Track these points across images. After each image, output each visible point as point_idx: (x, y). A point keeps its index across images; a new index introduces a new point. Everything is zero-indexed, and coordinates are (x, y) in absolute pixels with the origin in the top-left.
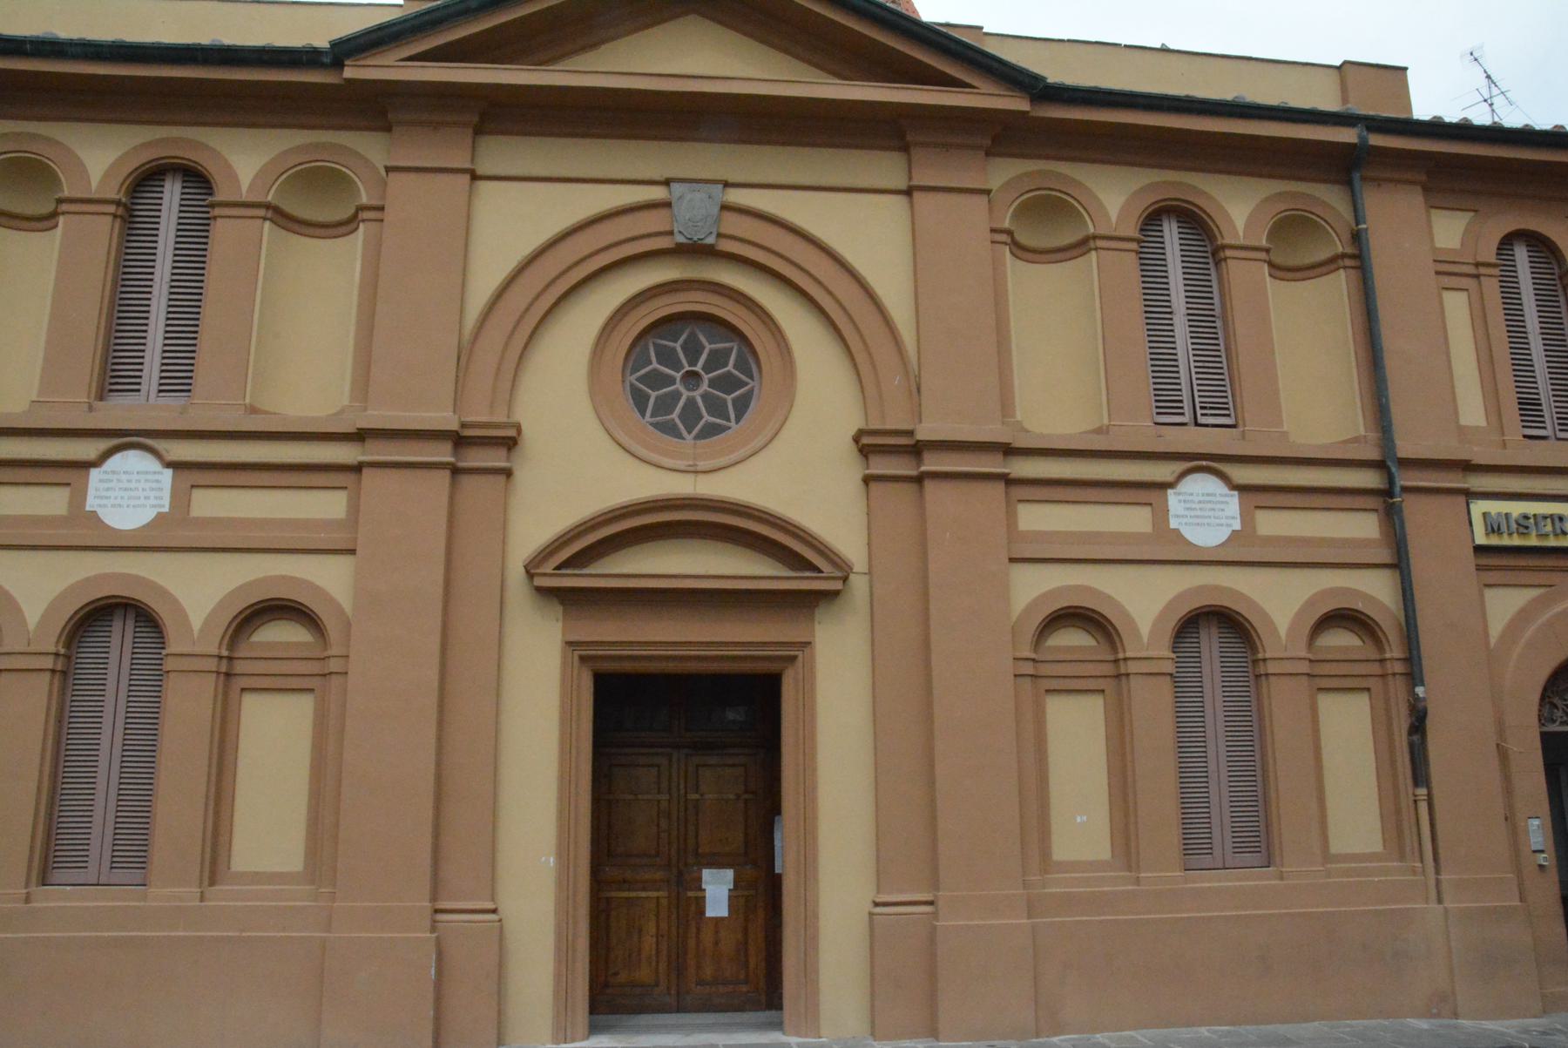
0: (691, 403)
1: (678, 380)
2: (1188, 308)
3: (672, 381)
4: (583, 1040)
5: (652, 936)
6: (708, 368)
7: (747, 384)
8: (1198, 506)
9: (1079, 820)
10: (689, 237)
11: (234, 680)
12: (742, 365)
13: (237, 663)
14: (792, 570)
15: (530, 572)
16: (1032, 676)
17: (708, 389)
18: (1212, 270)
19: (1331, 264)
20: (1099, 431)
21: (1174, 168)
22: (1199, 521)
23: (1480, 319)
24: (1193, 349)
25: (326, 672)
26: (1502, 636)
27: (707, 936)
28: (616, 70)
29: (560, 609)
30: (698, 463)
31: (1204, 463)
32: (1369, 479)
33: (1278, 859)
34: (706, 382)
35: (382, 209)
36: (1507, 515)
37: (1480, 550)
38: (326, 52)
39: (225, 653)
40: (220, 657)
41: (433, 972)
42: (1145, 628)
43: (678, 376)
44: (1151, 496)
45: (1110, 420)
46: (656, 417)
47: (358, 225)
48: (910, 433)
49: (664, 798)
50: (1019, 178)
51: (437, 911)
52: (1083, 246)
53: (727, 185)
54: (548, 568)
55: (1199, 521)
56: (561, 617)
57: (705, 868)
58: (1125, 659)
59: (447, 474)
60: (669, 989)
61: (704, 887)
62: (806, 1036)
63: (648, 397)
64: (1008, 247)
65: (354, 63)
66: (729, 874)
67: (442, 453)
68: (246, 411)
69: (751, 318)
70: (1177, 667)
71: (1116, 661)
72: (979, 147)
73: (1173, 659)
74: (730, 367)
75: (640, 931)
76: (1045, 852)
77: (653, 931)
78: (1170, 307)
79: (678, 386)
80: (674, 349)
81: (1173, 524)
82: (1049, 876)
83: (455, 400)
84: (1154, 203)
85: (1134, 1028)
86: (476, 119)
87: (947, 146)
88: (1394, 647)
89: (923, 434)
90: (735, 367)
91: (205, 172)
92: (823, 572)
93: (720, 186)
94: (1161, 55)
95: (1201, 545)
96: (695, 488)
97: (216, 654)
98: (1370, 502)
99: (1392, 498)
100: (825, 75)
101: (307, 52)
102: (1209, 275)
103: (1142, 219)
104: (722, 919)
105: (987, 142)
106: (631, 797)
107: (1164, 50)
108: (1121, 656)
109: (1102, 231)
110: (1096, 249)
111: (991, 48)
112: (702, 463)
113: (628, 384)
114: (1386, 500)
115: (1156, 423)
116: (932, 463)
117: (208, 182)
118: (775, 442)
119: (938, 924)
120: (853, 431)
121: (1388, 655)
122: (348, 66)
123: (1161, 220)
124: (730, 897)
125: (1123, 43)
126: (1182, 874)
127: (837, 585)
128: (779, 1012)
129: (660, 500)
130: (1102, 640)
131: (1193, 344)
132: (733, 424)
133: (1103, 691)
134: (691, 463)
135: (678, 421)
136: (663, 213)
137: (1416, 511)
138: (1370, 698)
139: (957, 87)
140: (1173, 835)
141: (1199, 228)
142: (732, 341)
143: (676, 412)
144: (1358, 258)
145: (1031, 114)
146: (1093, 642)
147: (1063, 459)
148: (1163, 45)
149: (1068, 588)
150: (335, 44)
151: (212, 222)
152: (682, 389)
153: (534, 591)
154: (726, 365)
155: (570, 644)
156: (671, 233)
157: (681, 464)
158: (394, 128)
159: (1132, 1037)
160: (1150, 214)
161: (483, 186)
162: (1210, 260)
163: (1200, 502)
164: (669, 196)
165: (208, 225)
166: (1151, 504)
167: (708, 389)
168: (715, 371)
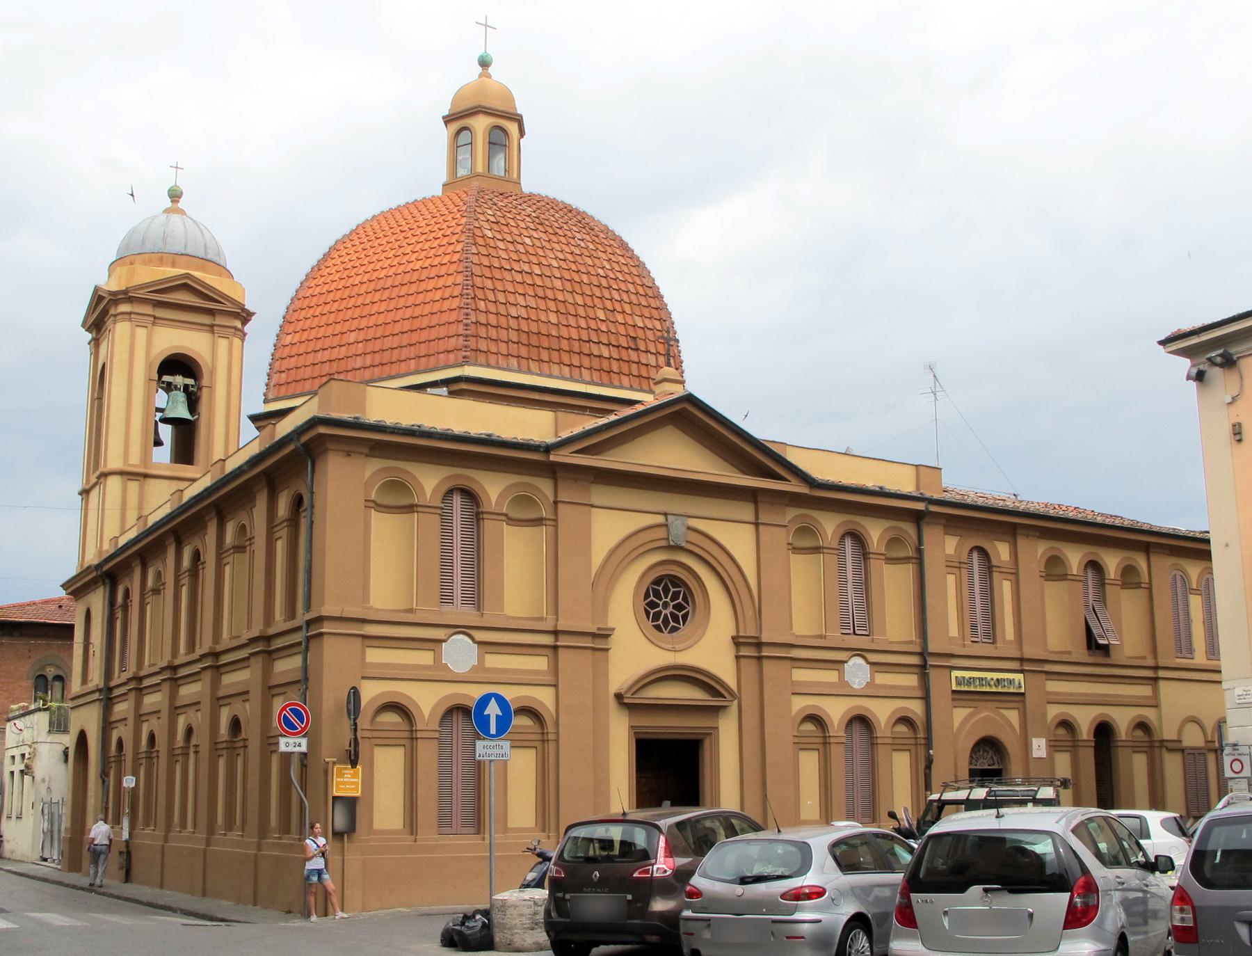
6: (672, 600)
12: (685, 599)
19: (906, 560)
21: (461, 467)
23: (959, 587)
26: (957, 730)
29: (627, 712)
30: (676, 646)
32: (915, 660)
33: (878, 819)
36: (964, 678)
37: (954, 692)
42: (427, 714)
44: (839, 666)
48: (757, 638)
52: (410, 508)
63: (650, 613)
67: (547, 640)
69: (696, 585)
71: (543, 734)
88: (921, 733)
89: (764, 640)
98: (916, 670)
99: (926, 670)
114: (922, 669)
121: (918, 736)
123: (452, 494)
130: (911, 730)
137: (933, 674)
138: (405, 750)
142: (680, 587)
144: (919, 559)
149: (384, 693)
157: (669, 647)
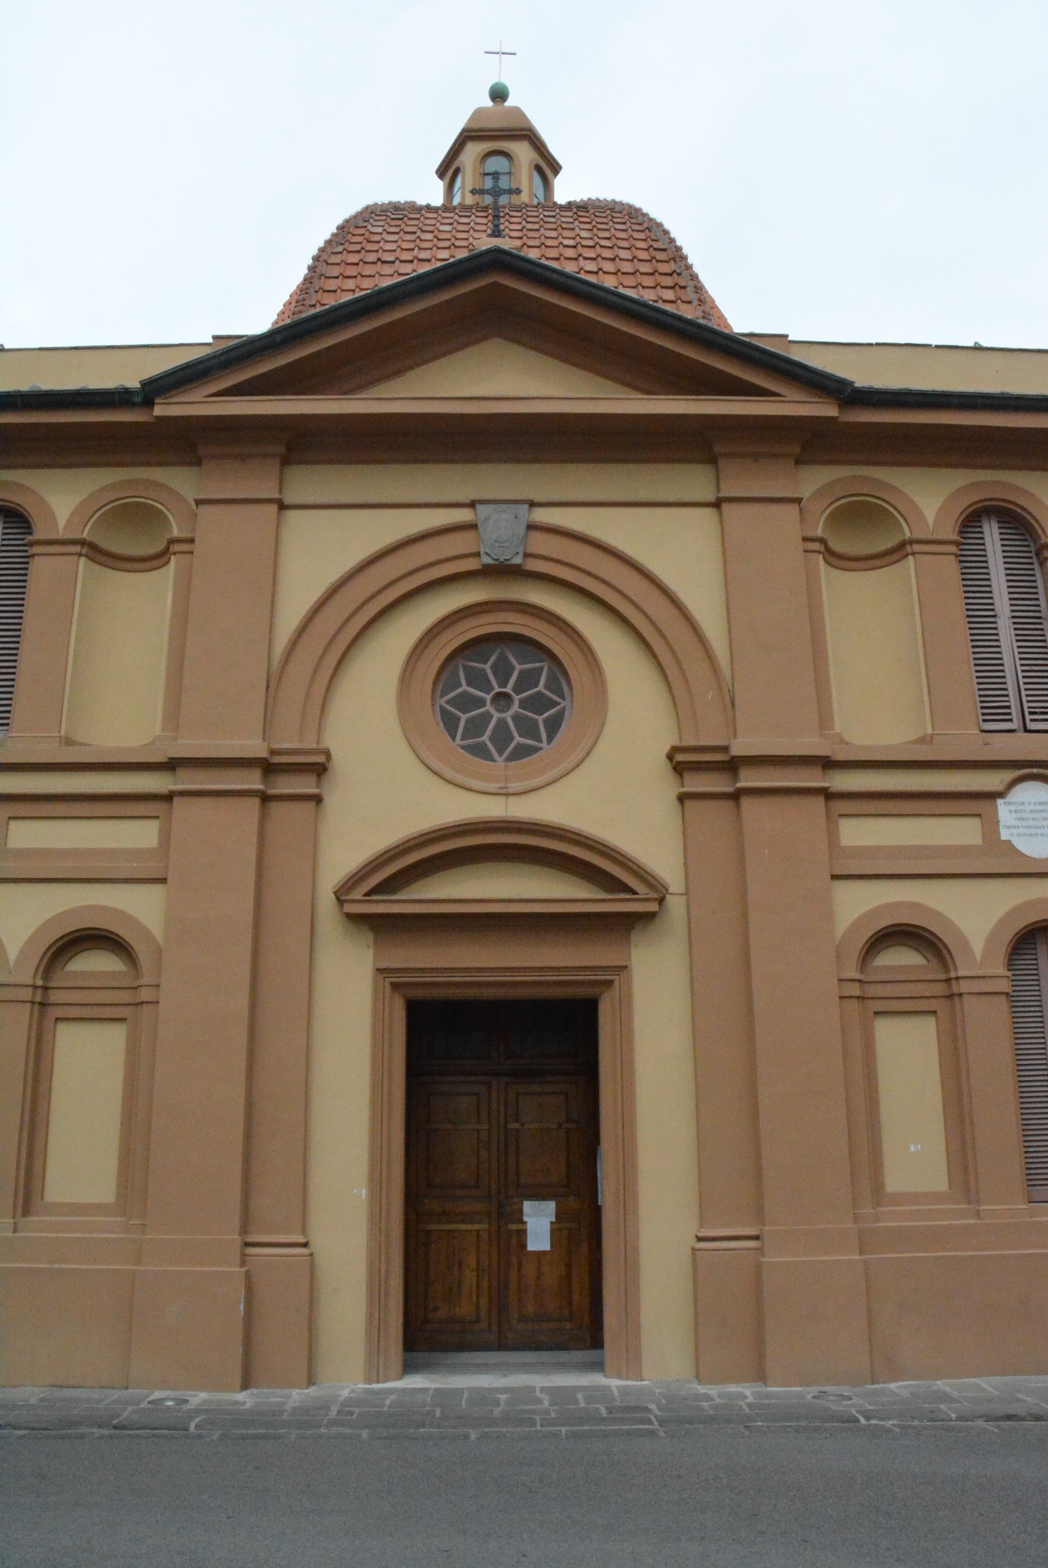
0: (502, 724)
1: (488, 702)
2: (1012, 611)
3: (481, 703)
4: (397, 1379)
5: (472, 1271)
6: (518, 689)
7: (558, 704)
8: (1030, 816)
9: (912, 1149)
10: (495, 557)
11: (51, 1009)
12: (553, 684)
13: (51, 992)
14: (607, 892)
15: (341, 895)
16: (858, 997)
17: (518, 710)
18: (1036, 570)
20: (923, 740)
22: (1033, 831)
24: (1019, 653)
25: (138, 1001)
27: (530, 1269)
28: (407, 396)
29: (369, 937)
30: (509, 785)
31: (1035, 771)
34: (516, 703)
35: (192, 541)
38: (137, 392)
39: (40, 983)
40: (35, 987)
41: (242, 1307)
42: (977, 947)
43: (488, 697)
45: (933, 730)
46: (468, 739)
47: (170, 558)
48: (725, 749)
49: (484, 1127)
50: (832, 485)
51: (247, 1245)
52: (899, 551)
53: (532, 504)
54: (358, 894)
55: (1033, 831)
56: (372, 944)
57: (527, 1200)
58: (957, 978)
59: (257, 801)
60: (490, 1325)
61: (525, 1219)
62: (627, 1379)
64: (821, 556)
65: (163, 401)
66: (551, 1206)
67: (253, 781)
68: (60, 743)
69: (561, 638)
70: (1013, 986)
72: (786, 456)
73: (1008, 977)
74: (541, 687)
75: (460, 1264)
76: (878, 1185)
77: (474, 1265)
78: (993, 610)
79: (489, 707)
80: (484, 670)
81: (1004, 835)
82: (882, 1209)
83: (264, 728)
84: (971, 505)
85: (980, 1374)
86: (282, 449)
87: (756, 457)
89: (737, 750)
90: (546, 687)
91: (25, 513)
92: (637, 894)
93: (526, 506)
94: (972, 353)
95: (1035, 857)
96: (506, 810)
97: (32, 984)
100: (622, 388)
101: (119, 392)
102: (1034, 575)
103: (960, 521)
104: (544, 1253)
105: (797, 450)
106: (450, 1127)
107: (978, 348)
108: (953, 975)
109: (917, 536)
110: (913, 554)
111: (797, 355)
112: (514, 785)
113: (438, 705)
115: (982, 731)
116: (748, 779)
117: (27, 522)
118: (588, 761)
119: (764, 1260)
120: (666, 749)
122: (158, 404)
124: (552, 1231)
125: (934, 343)
126: (1025, 1207)
127: (653, 907)
128: (598, 1352)
129: (481, 822)
131: (1019, 647)
132: (544, 744)
133: (935, 1012)
134: (502, 785)
135: (488, 743)
136: (469, 535)
139: (762, 396)
140: (1015, 1164)
141: (1021, 527)
142: (543, 661)
143: (486, 734)
145: (839, 420)
146: (924, 962)
147: (943, 771)
148: (976, 343)
149: (887, 907)
150: (144, 384)
151: (30, 560)
152: (493, 711)
153: (345, 917)
154: (536, 685)
155: (380, 971)
156: (478, 555)
157: (493, 787)
158: (204, 463)
159: (976, 1385)
160: (967, 517)
161: (292, 515)
162: (1035, 560)
163: (1032, 811)
164: (474, 518)
165: (27, 563)
166: (980, 815)
167: (518, 710)
168: (528, 690)
